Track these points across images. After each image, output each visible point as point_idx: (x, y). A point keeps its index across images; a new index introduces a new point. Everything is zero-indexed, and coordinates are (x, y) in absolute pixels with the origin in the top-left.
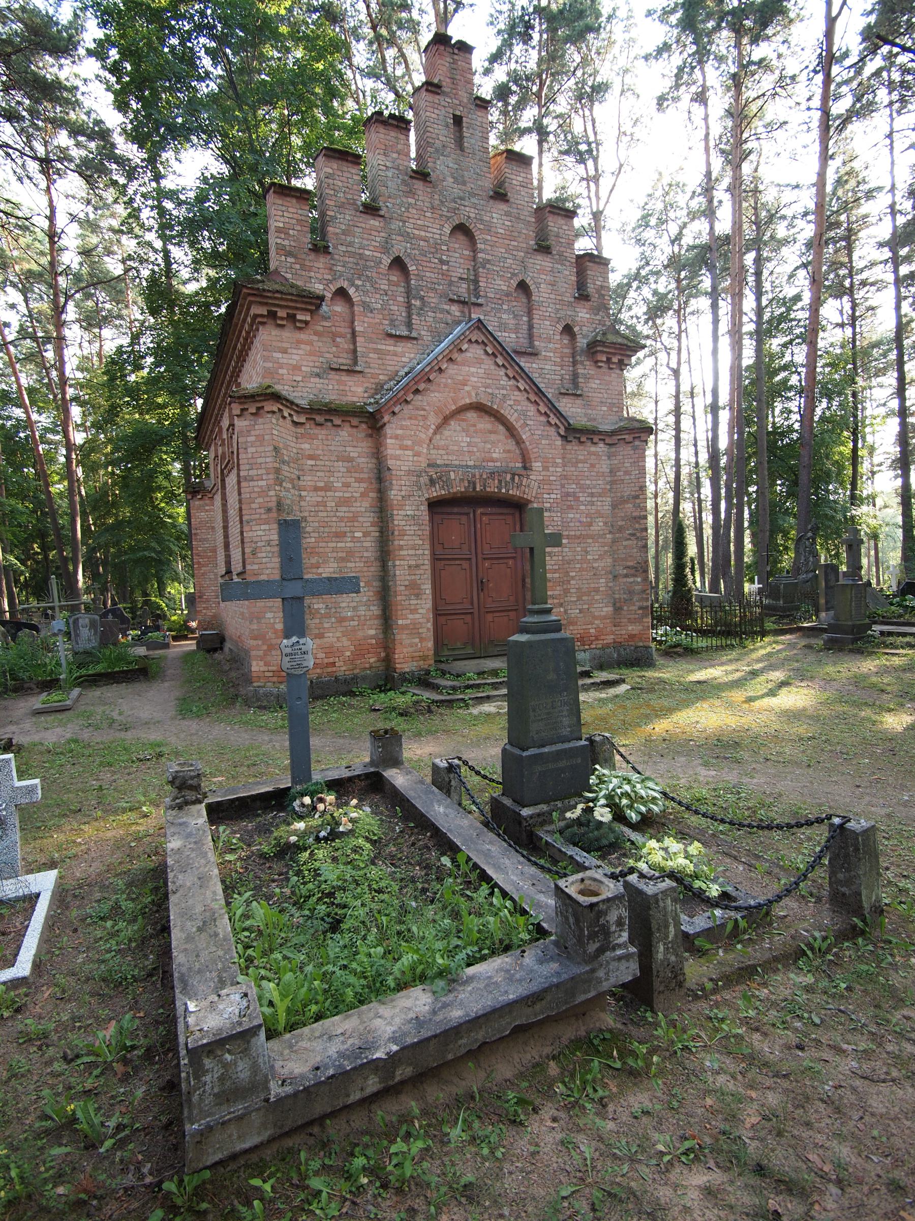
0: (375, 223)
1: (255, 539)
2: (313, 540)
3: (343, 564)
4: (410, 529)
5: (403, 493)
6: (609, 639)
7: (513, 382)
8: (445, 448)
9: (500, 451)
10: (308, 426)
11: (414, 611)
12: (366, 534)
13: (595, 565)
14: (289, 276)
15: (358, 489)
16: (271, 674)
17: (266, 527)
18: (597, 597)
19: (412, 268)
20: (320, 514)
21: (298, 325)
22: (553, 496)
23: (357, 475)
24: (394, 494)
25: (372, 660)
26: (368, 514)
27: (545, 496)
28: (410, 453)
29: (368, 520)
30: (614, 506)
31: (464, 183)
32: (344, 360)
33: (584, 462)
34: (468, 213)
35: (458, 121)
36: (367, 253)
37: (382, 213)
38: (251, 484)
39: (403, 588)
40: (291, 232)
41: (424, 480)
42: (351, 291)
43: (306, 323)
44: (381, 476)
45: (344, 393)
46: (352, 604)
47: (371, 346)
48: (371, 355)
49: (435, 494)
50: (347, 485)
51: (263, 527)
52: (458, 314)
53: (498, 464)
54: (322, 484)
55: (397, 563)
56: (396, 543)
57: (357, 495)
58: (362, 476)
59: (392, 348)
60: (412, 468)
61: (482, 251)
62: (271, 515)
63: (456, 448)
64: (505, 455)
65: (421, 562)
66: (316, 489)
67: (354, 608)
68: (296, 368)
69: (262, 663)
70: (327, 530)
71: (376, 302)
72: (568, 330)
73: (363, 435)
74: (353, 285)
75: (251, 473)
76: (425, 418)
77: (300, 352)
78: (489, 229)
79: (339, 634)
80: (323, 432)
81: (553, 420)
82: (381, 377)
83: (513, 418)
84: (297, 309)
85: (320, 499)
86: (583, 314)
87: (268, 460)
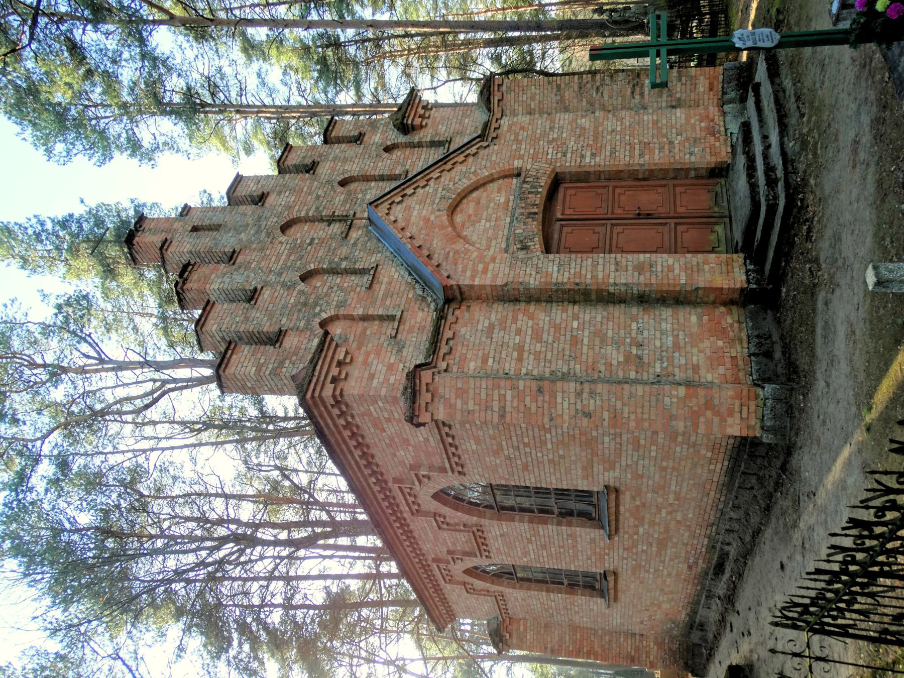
0: (266, 294)
1: (573, 413)
2: (578, 366)
3: (609, 341)
4: (574, 268)
5: (534, 273)
6: (714, 111)
7: (432, 183)
8: (489, 240)
9: (500, 195)
10: (451, 362)
11: (671, 269)
12: (576, 317)
13: (628, 123)
14: (301, 366)
15: (523, 321)
16: (745, 409)
17: (559, 395)
18: (664, 122)
19: (312, 267)
20: (549, 357)
21: (348, 360)
22: (550, 151)
23: (509, 322)
24: (534, 281)
25: (730, 320)
26: (553, 315)
27: (550, 156)
28: (491, 266)
29: (559, 314)
30: (566, 110)
31: (248, 225)
32: (389, 329)
33: (517, 135)
34: (274, 221)
35: (195, 229)
36: (292, 301)
37: (259, 287)
38: (508, 409)
39: (642, 278)
40: (262, 361)
41: (521, 254)
42: (324, 316)
43: (347, 353)
44: (511, 296)
45: (421, 329)
46: (658, 336)
47: (378, 303)
48: (388, 303)
49: (538, 246)
50: (519, 332)
51: (559, 400)
52: (360, 232)
53: (512, 198)
54: (515, 354)
55: (612, 281)
56: (588, 281)
57: (530, 323)
58: (510, 317)
59: (383, 286)
60: (508, 264)
61: (307, 213)
62: (546, 389)
63: (491, 232)
64: (503, 192)
65: (612, 261)
66: (520, 359)
67: (662, 334)
68: (390, 368)
69: (730, 420)
70: (567, 353)
71: (336, 297)
72: (388, 149)
73: (467, 315)
74: (319, 314)
75: (496, 408)
76: (456, 252)
77: (375, 362)
78: (289, 208)
79: (695, 351)
80: (459, 348)
81: (473, 150)
82: (410, 296)
83: (466, 183)
84: (332, 358)
85: (532, 357)
86: (376, 138)
87: (484, 386)
